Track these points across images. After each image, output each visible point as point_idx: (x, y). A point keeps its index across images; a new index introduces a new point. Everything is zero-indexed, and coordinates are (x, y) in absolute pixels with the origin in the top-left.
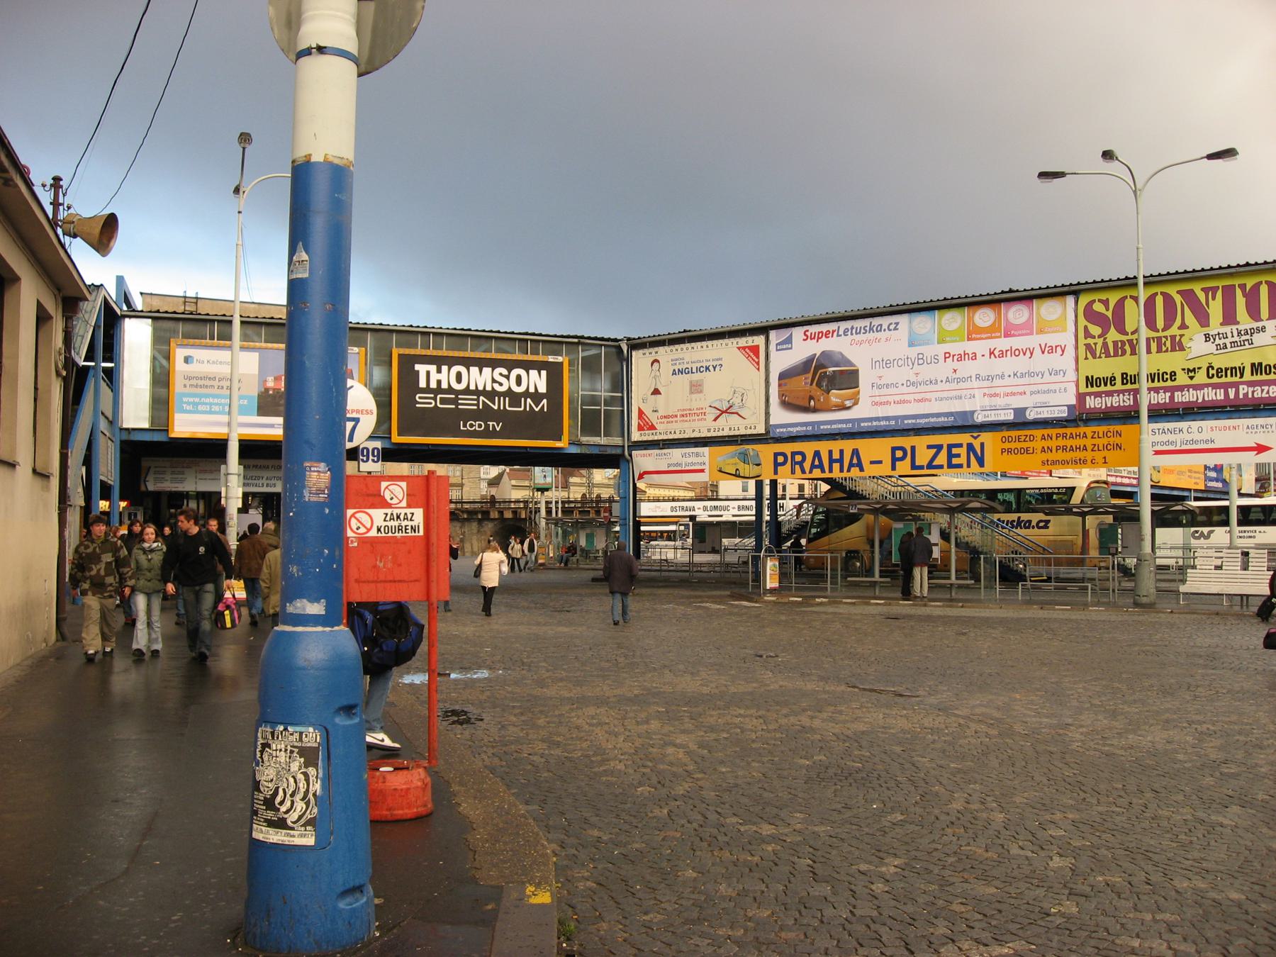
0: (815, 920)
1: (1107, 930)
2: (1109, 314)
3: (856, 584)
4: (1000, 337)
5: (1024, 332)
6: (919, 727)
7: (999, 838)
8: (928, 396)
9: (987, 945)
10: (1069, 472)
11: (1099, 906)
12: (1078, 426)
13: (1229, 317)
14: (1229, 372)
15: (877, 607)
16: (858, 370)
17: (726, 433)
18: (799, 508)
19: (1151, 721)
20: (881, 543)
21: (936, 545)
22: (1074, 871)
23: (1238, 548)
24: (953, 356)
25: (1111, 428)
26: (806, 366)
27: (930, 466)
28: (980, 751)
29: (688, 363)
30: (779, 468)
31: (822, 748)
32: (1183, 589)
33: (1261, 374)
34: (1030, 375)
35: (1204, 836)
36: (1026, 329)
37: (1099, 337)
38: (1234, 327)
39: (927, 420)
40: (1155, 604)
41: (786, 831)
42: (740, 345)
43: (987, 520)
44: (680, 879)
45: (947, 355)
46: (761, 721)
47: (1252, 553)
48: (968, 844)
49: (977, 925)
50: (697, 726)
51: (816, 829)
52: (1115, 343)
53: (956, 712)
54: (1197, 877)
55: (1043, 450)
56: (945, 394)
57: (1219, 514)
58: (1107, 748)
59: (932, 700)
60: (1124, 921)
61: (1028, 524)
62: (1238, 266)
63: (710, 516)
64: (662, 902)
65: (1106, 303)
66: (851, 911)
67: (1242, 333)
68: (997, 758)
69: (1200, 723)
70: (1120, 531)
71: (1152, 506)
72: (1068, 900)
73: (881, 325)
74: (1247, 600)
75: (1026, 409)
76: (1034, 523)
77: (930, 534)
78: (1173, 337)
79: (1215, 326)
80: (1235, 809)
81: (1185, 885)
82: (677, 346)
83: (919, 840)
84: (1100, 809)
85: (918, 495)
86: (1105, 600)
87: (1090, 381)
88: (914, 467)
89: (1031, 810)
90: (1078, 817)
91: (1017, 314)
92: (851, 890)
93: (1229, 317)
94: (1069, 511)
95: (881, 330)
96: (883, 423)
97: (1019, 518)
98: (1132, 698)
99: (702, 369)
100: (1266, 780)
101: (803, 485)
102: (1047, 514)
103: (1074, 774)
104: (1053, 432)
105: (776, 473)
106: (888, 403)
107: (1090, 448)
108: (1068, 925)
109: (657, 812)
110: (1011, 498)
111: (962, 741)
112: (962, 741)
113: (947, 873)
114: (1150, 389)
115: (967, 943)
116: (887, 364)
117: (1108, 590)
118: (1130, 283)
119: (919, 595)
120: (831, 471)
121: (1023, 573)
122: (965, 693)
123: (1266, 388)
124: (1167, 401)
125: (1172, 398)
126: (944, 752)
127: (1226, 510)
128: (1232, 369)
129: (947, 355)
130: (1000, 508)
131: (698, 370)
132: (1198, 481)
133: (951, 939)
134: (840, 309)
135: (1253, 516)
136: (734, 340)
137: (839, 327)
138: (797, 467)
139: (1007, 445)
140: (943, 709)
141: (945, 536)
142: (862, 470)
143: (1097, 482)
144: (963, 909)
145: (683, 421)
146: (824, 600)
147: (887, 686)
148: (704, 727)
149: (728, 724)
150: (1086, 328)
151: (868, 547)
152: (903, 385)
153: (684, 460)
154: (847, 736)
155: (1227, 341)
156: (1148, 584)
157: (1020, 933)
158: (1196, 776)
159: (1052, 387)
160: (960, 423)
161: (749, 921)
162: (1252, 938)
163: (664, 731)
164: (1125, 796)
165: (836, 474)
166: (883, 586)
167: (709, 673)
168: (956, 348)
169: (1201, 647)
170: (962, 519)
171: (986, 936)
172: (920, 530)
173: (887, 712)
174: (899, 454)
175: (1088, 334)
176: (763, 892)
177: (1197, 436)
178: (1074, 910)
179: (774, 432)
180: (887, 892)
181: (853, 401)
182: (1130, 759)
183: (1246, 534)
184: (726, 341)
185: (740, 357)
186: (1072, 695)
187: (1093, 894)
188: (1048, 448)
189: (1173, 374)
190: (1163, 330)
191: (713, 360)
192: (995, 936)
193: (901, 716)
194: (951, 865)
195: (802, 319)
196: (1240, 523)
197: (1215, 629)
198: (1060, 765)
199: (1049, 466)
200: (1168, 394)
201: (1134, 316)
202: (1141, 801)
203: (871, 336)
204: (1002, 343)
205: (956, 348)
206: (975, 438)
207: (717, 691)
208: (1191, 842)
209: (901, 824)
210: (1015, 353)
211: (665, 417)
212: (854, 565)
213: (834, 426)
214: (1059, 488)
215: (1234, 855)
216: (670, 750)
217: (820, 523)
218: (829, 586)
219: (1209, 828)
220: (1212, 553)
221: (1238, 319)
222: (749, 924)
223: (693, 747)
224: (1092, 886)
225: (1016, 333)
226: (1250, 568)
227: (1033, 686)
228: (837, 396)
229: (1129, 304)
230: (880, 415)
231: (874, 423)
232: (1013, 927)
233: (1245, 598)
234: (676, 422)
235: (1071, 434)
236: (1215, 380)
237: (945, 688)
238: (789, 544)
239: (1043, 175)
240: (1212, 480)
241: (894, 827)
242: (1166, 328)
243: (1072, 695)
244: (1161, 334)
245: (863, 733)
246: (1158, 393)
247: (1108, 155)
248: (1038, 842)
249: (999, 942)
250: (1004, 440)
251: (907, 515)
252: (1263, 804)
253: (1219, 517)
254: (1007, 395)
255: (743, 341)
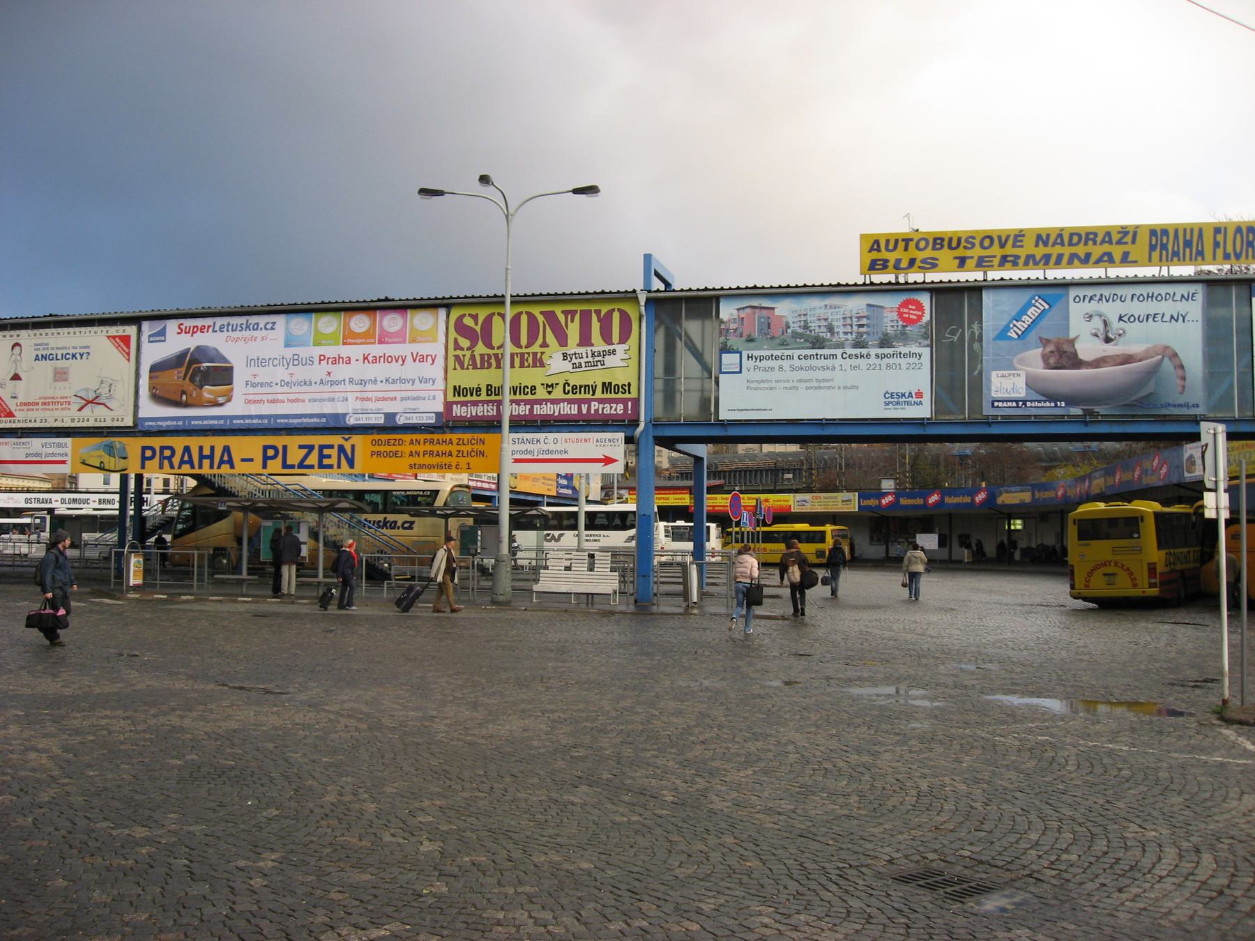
0: (196, 919)
1: (474, 905)
2: (478, 329)
3: (223, 582)
4: (374, 343)
5: (397, 340)
6: (291, 724)
7: (372, 827)
8: (300, 396)
9: (364, 929)
10: (434, 476)
11: (467, 885)
12: (444, 433)
13: (585, 340)
14: (583, 389)
15: (244, 604)
16: (231, 369)
17: (91, 423)
18: (165, 503)
19: (509, 712)
20: (250, 540)
21: (305, 543)
22: (443, 853)
23: (585, 551)
24: (328, 358)
25: (475, 436)
26: (179, 360)
27: (301, 466)
28: (350, 745)
29: (52, 349)
30: (147, 462)
31: (193, 747)
32: (536, 588)
33: (611, 393)
34: (401, 382)
35: (557, 814)
36: (400, 337)
37: (468, 349)
38: (589, 349)
39: (299, 421)
40: (510, 602)
41: (160, 832)
42: (110, 334)
43: (355, 520)
44: (49, 889)
45: (322, 358)
46: (130, 722)
47: (597, 554)
48: (343, 835)
49: (354, 910)
50: (59, 730)
51: (191, 828)
52: (482, 356)
53: (326, 708)
54: (553, 852)
55: (411, 454)
56: (318, 396)
57: (569, 519)
58: (469, 738)
59: (303, 697)
60: (489, 896)
61: (393, 525)
62: (595, 293)
63: (68, 509)
64: (30, 915)
65: (475, 317)
66: (231, 908)
67: (596, 354)
68: (367, 750)
69: (552, 711)
70: (479, 533)
71: (510, 510)
72: (438, 881)
73: (258, 324)
74: (592, 598)
75: (395, 414)
76: (399, 524)
77: (299, 532)
78: (535, 354)
79: (572, 347)
80: (584, 788)
81: (543, 859)
82: (41, 331)
83: (294, 834)
84: (464, 794)
85: (287, 493)
86: (466, 598)
87: (457, 391)
88: (285, 466)
89: (400, 799)
90: (444, 803)
91: (392, 322)
92: (230, 887)
93: (585, 340)
94: (433, 513)
95: (257, 329)
96: (255, 421)
97: (385, 518)
98: (491, 690)
99: (68, 357)
100: (610, 761)
101: (169, 479)
102: (412, 516)
103: (440, 763)
104: (421, 437)
105: (143, 467)
106: (261, 401)
107: (455, 454)
108: (439, 905)
109: (20, 821)
110: (378, 499)
111: (333, 736)
112: (333, 736)
113: (324, 863)
114: (512, 401)
115: (346, 929)
116: (262, 362)
117: (468, 588)
118: (498, 301)
119: (286, 592)
120: (200, 467)
121: (388, 572)
122: (333, 689)
123: (614, 406)
124: (527, 413)
125: (531, 410)
126: (316, 746)
127: (574, 515)
128: (586, 386)
129: (322, 358)
130: (368, 508)
131: (64, 357)
132: (551, 487)
133: (330, 927)
134: (217, 305)
135: (598, 521)
136: (104, 329)
137: (215, 323)
138: (166, 462)
139: (377, 449)
140: (312, 705)
141: (314, 535)
142: (232, 467)
143: (460, 486)
144: (340, 896)
145: (45, 409)
146: (190, 597)
147: (257, 684)
148: (68, 730)
149: (94, 726)
150: (456, 340)
151: (235, 545)
152: (277, 384)
153: (44, 450)
154: (219, 735)
155: (582, 361)
156: (505, 582)
157: (395, 915)
158: (549, 760)
159: (422, 394)
160: (332, 425)
161: (126, 926)
162: (601, 901)
163: (25, 736)
164: (487, 782)
165: (206, 470)
166: (251, 584)
167: (71, 673)
168: (331, 351)
169: (552, 642)
170: (332, 518)
171: (362, 921)
172: (289, 529)
173: (258, 709)
174: (271, 452)
175: (457, 346)
176: (139, 895)
177: (552, 447)
178: (445, 889)
179: (143, 426)
180: (265, 886)
181: (226, 398)
182: (490, 747)
183: (592, 538)
184: (95, 329)
185: (109, 347)
186: (436, 688)
187: (460, 873)
188: (416, 452)
189: (533, 388)
190: (526, 347)
191: (80, 348)
192: (372, 920)
193: (272, 713)
194: (327, 856)
195: (177, 312)
196: (587, 528)
197: (564, 625)
198: (427, 756)
199: (416, 469)
200: (528, 407)
201: (501, 331)
202: (501, 786)
203: (247, 334)
204: (376, 350)
205: (331, 351)
206: (346, 440)
207: (80, 692)
208: (546, 821)
209: (276, 819)
210: (389, 359)
211: (25, 404)
212: (221, 562)
213: (205, 422)
214: (424, 491)
215: (584, 829)
216: (32, 755)
217: (187, 519)
218: (195, 583)
219: (561, 807)
220: (562, 554)
221: (593, 341)
222: (127, 928)
223: (57, 750)
224: (460, 867)
225: (389, 340)
226: (596, 569)
227: (400, 681)
228: (210, 392)
229: (497, 320)
230: (253, 414)
231: (247, 421)
232: (389, 910)
233: (590, 596)
234: (37, 410)
235: (438, 440)
236: (571, 396)
237: (315, 685)
238: (153, 539)
239: (424, 192)
240: (563, 487)
241: (271, 822)
242: (529, 345)
243: (436, 688)
244: (524, 350)
245: (235, 731)
246: (519, 405)
247: (484, 179)
248: (408, 829)
249: (378, 926)
250: (374, 443)
251: (275, 514)
252: (607, 783)
253: (567, 522)
254: (378, 399)
255: (113, 330)
